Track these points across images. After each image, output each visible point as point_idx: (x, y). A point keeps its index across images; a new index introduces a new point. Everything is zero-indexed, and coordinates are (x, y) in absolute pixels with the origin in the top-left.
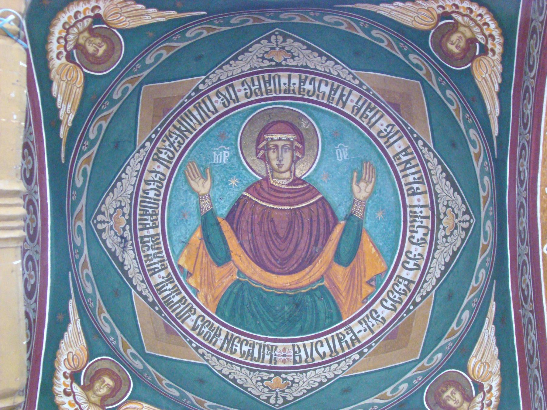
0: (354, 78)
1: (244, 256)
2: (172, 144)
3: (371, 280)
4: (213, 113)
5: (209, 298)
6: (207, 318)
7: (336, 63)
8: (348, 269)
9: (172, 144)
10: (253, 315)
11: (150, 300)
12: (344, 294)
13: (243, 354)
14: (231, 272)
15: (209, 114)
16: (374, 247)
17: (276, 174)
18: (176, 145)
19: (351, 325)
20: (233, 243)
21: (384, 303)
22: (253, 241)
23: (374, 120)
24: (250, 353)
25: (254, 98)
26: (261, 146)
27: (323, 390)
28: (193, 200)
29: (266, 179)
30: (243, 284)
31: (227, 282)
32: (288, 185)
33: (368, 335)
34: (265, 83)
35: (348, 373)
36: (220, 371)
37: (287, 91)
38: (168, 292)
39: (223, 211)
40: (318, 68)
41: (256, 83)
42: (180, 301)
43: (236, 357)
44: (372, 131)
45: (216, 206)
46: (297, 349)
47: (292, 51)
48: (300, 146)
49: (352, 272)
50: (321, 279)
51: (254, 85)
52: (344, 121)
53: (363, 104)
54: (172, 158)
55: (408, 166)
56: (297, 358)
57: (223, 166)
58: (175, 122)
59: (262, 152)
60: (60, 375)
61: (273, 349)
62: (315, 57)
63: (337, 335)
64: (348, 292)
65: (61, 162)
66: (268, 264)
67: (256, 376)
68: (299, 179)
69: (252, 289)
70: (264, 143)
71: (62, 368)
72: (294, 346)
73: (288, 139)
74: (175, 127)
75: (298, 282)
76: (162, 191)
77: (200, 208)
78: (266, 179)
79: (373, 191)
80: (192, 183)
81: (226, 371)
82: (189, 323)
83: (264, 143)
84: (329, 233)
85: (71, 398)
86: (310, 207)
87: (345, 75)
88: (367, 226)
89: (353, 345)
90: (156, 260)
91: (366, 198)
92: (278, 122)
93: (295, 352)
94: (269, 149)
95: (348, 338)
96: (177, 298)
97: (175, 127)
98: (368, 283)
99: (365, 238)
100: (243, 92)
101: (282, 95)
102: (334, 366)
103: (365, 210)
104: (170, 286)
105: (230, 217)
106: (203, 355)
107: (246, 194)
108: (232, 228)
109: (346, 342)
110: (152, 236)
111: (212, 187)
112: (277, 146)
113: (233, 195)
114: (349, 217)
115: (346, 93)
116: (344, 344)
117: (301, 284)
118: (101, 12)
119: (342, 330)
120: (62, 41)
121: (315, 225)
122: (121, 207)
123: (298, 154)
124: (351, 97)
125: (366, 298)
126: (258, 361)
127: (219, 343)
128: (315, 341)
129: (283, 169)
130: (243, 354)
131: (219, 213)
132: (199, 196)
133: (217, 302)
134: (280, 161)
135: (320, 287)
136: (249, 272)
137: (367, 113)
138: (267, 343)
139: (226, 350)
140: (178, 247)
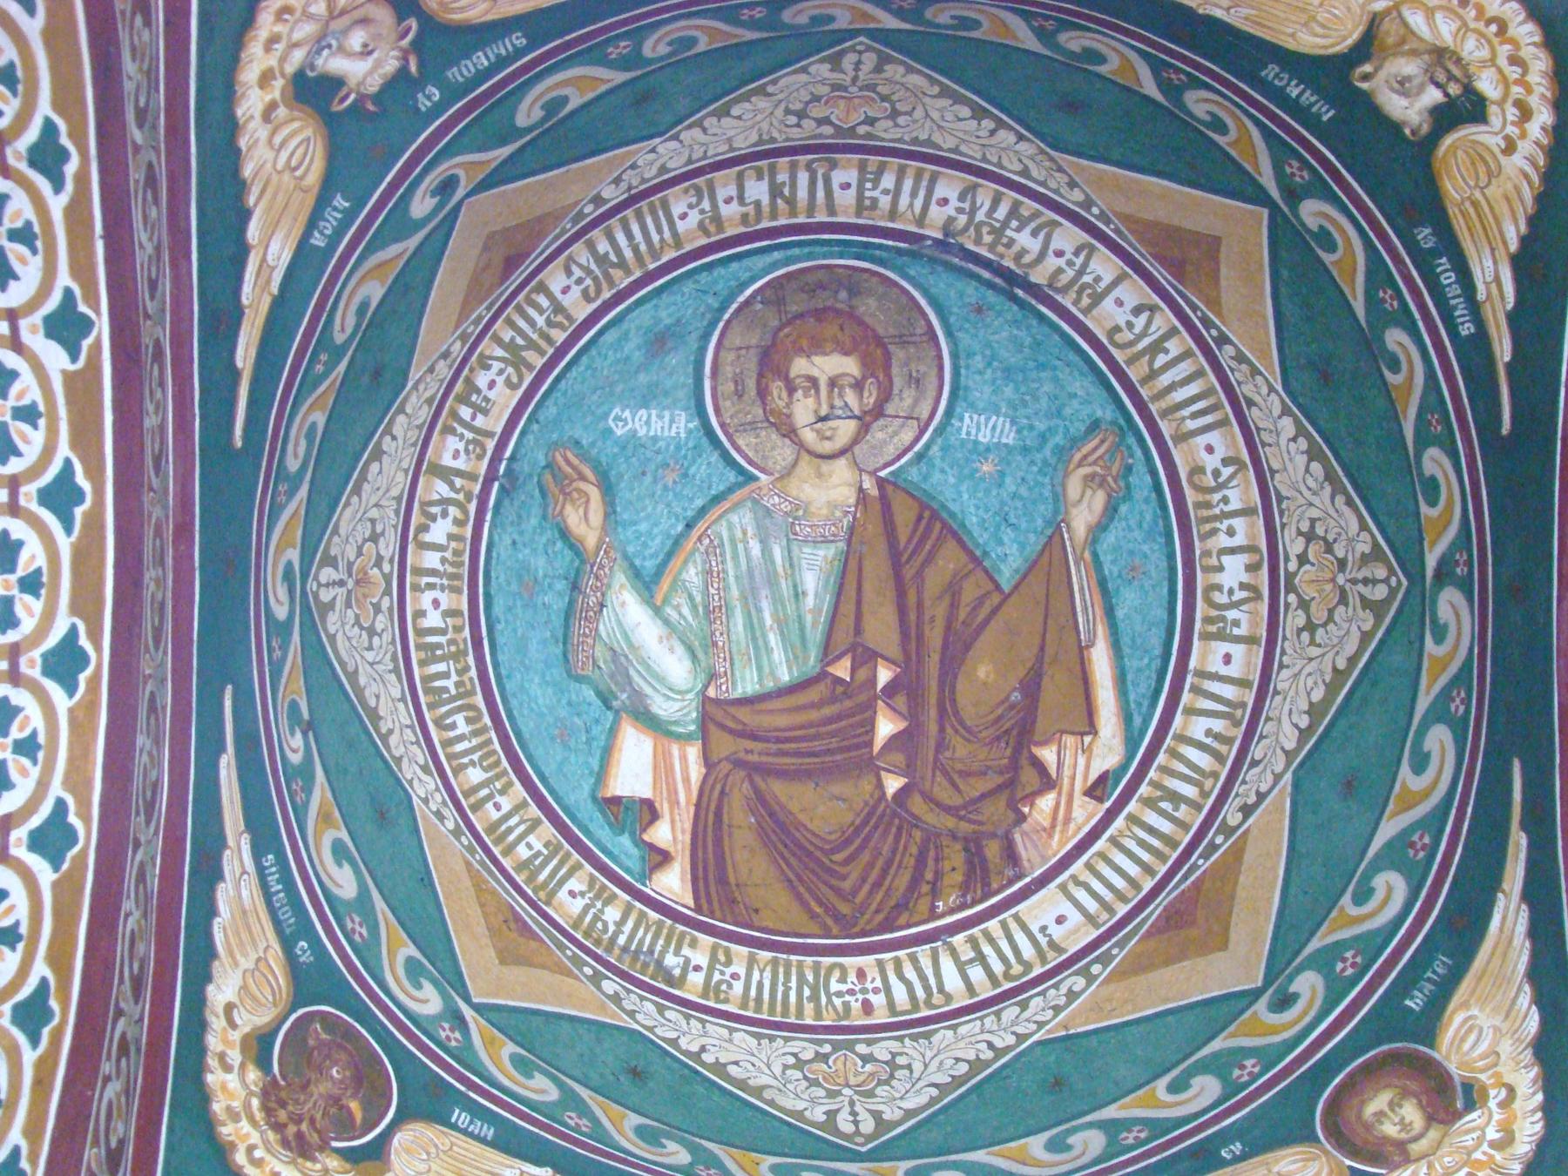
35: (641, 149)
47: (894, 98)
55: (1161, 360)
62: (960, 120)
65: (513, 117)
67: (782, 1050)
86: (951, 544)
102: (1010, 1013)
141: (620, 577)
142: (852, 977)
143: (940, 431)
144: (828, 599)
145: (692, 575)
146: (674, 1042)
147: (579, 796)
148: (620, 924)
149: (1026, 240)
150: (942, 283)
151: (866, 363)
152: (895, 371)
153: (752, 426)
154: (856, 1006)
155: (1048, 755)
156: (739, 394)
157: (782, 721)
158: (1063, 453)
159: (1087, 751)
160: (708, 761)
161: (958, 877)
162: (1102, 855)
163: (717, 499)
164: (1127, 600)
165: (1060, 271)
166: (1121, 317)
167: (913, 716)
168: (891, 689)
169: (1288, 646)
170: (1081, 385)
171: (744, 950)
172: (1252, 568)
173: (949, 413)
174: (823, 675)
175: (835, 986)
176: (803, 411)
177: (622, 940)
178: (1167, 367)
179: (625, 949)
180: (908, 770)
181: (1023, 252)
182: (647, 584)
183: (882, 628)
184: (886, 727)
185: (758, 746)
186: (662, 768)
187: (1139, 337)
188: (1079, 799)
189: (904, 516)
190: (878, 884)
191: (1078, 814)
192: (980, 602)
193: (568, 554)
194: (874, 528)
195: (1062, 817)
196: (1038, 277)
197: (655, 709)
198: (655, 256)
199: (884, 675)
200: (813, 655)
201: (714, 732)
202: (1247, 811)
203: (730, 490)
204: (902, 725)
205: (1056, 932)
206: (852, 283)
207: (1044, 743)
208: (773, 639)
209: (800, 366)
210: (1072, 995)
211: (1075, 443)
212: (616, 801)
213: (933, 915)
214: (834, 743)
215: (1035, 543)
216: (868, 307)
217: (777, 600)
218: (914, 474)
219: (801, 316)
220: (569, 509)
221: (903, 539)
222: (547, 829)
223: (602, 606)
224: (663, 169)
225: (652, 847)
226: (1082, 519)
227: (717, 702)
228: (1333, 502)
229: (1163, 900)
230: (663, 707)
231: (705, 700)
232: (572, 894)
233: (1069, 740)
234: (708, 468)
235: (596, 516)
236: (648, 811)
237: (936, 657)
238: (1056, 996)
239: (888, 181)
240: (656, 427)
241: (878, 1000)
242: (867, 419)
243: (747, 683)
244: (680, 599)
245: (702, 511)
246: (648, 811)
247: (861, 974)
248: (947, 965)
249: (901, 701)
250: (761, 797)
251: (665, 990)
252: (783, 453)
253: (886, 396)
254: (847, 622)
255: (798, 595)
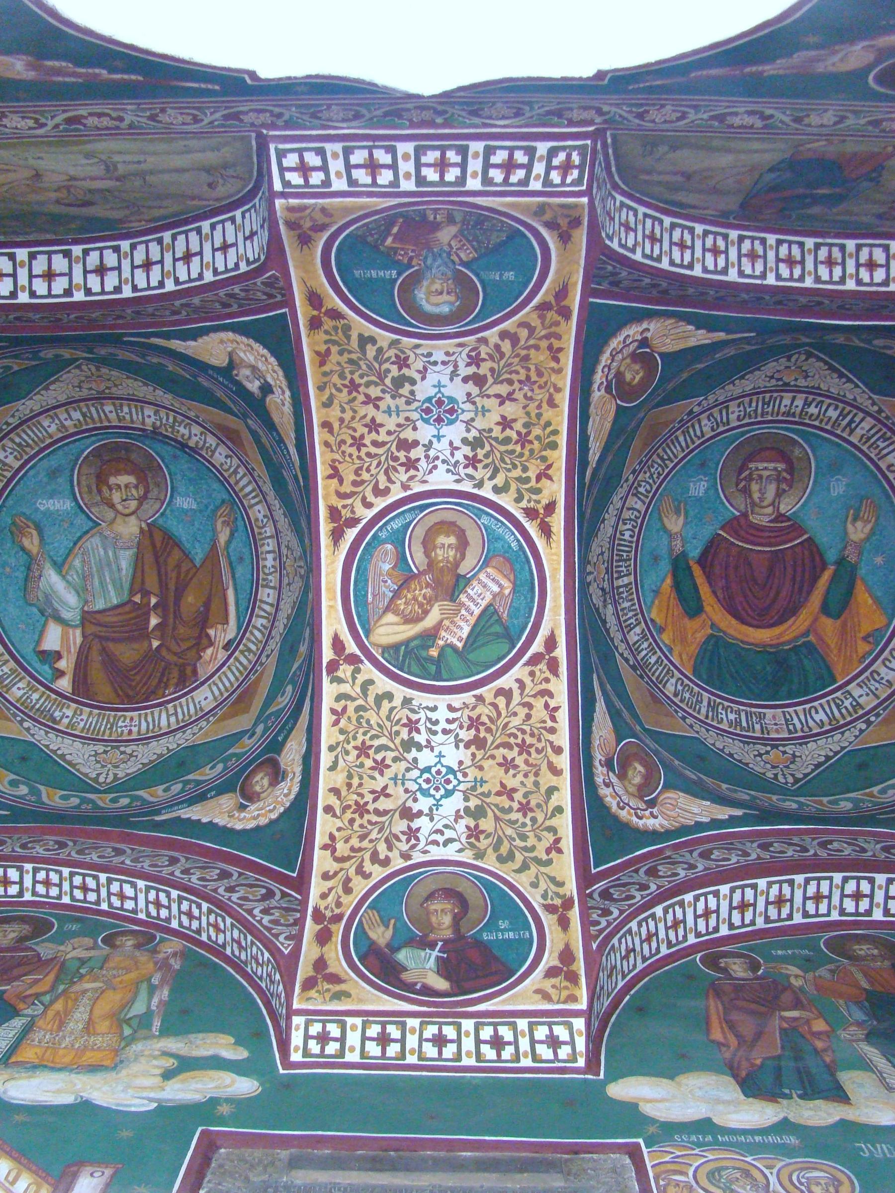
0: (874, 404)
1: (717, 607)
2: (651, 476)
3: (868, 635)
4: (699, 438)
5: (684, 657)
6: (686, 681)
7: (857, 386)
8: (839, 622)
9: (651, 476)
10: (732, 676)
11: (631, 663)
12: (835, 651)
13: (730, 724)
14: (703, 627)
15: (695, 439)
16: (871, 596)
17: (757, 509)
18: (655, 476)
19: (848, 688)
20: (705, 590)
21: (887, 663)
22: (726, 588)
23: (885, 452)
24: (738, 722)
25: (746, 421)
26: (743, 475)
27: (831, 765)
28: (665, 540)
29: (745, 515)
30: (718, 638)
31: (701, 636)
32: (770, 521)
33: (872, 701)
34: (764, 404)
36: (713, 745)
37: (788, 414)
38: (644, 653)
39: (695, 553)
40: (832, 390)
41: (754, 404)
42: (657, 662)
43: (724, 726)
44: (880, 463)
45: (688, 547)
46: (788, 717)
48: (788, 477)
49: (844, 625)
50: (806, 633)
51: (750, 406)
52: (847, 451)
53: (877, 433)
54: (649, 492)
56: (791, 727)
57: (699, 500)
58: (660, 450)
59: (743, 483)
60: (597, 763)
61: (761, 717)
63: (833, 699)
64: (840, 650)
66: (746, 617)
68: (783, 515)
69: (728, 645)
70: (747, 472)
71: (598, 756)
72: (784, 713)
73: (775, 469)
74: (658, 455)
75: (781, 635)
76: (637, 530)
77: (671, 550)
78: (745, 515)
79: (872, 532)
80: (665, 520)
81: (719, 745)
82: (670, 689)
83: (747, 472)
84: (815, 579)
85: (611, 789)
86: (176, 549)
87: (863, 400)
88: (862, 571)
89: (856, 712)
90: (630, 614)
91: (862, 540)
92: (768, 449)
93: (786, 720)
94: (751, 479)
95: (847, 703)
96: (653, 660)
97: (658, 455)
98: (865, 639)
99: (860, 588)
100: (736, 414)
101: (780, 418)
103: (860, 554)
104: (645, 645)
105: (702, 561)
106: (691, 726)
107: (721, 532)
108: (704, 572)
109: (846, 708)
110: (626, 586)
111: (685, 524)
112: (761, 477)
113: (707, 532)
114: (841, 561)
115: (857, 419)
116: (844, 711)
117: (782, 640)
118: (649, 335)
119: (838, 694)
120: (606, 370)
121: (799, 569)
122: (602, 553)
123: (784, 486)
124: (863, 424)
125: (863, 657)
126: (748, 731)
127: (704, 711)
128: (807, 706)
129: (765, 503)
130: (730, 724)
131: (691, 555)
132: (671, 536)
133: (692, 662)
134: (763, 494)
135: (804, 643)
136: (722, 625)
137: (879, 443)
138: (753, 710)
139: (713, 720)
140: (650, 597)
141: (48, 565)
142: (128, 720)
143: (168, 505)
144: (131, 571)
145: (77, 563)
146: (47, 746)
147: (28, 650)
148: (38, 700)
149: (182, 430)
150: (158, 446)
151: (138, 478)
152: (149, 480)
153: (97, 504)
154: (126, 731)
155: (211, 632)
156: (90, 492)
157: (115, 619)
158: (215, 511)
159: (225, 631)
160: (84, 636)
161: (175, 680)
162: (224, 673)
163: (87, 532)
164: (240, 570)
165: (197, 442)
166: (223, 460)
167: (165, 617)
168: (156, 606)
169: (284, 590)
170: (216, 486)
171: (88, 710)
172: (275, 559)
173: (172, 496)
174: (130, 601)
175: (120, 724)
176: (116, 497)
177: (37, 706)
178: (241, 478)
179: (38, 710)
180: (161, 638)
181: (183, 435)
182: (59, 567)
183: (152, 582)
184: (154, 621)
185: (104, 629)
186: (65, 638)
187: (230, 467)
188: (221, 650)
189: (158, 537)
190: (145, 684)
191: (219, 656)
192: (188, 571)
193: (25, 556)
194: (147, 542)
195: (213, 658)
196: (192, 444)
197: (63, 616)
198: (43, 442)
199: (153, 601)
200: (126, 592)
201: (87, 624)
202: (268, 656)
203: (91, 529)
204: (160, 620)
205: (203, 703)
206: (127, 448)
207: (211, 627)
208: (110, 587)
209: (112, 480)
210: (201, 729)
211: (218, 508)
212: (43, 652)
213: (164, 696)
214: (134, 627)
215: (207, 547)
216: (133, 456)
217: (111, 571)
218: (161, 522)
219: (109, 461)
220: (24, 539)
221: (158, 545)
222: (12, 664)
223: (40, 576)
224: (32, 411)
225: (58, 670)
226: (223, 538)
227: (87, 612)
228: (772, 449)
229: (238, 692)
230: (66, 615)
231: (84, 612)
232: (19, 689)
233: (220, 627)
234: (80, 520)
235: (36, 541)
236: (58, 656)
237: (172, 594)
238: (196, 729)
239: (126, 409)
240: (58, 506)
241: (135, 729)
242: (142, 500)
243: (100, 605)
244: (73, 572)
245: (80, 538)
246: (58, 656)
247: (132, 719)
248: (164, 716)
249: (159, 611)
250: (104, 649)
251: (51, 725)
252: (110, 514)
253: (147, 492)
254: (139, 580)
255: (119, 570)
